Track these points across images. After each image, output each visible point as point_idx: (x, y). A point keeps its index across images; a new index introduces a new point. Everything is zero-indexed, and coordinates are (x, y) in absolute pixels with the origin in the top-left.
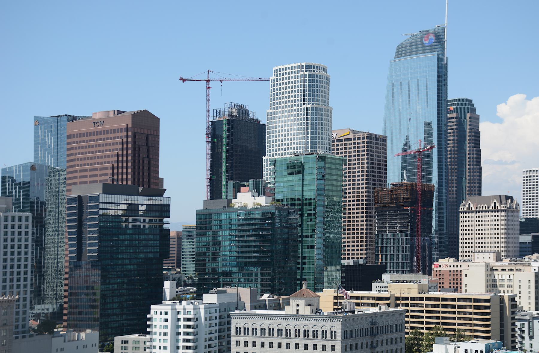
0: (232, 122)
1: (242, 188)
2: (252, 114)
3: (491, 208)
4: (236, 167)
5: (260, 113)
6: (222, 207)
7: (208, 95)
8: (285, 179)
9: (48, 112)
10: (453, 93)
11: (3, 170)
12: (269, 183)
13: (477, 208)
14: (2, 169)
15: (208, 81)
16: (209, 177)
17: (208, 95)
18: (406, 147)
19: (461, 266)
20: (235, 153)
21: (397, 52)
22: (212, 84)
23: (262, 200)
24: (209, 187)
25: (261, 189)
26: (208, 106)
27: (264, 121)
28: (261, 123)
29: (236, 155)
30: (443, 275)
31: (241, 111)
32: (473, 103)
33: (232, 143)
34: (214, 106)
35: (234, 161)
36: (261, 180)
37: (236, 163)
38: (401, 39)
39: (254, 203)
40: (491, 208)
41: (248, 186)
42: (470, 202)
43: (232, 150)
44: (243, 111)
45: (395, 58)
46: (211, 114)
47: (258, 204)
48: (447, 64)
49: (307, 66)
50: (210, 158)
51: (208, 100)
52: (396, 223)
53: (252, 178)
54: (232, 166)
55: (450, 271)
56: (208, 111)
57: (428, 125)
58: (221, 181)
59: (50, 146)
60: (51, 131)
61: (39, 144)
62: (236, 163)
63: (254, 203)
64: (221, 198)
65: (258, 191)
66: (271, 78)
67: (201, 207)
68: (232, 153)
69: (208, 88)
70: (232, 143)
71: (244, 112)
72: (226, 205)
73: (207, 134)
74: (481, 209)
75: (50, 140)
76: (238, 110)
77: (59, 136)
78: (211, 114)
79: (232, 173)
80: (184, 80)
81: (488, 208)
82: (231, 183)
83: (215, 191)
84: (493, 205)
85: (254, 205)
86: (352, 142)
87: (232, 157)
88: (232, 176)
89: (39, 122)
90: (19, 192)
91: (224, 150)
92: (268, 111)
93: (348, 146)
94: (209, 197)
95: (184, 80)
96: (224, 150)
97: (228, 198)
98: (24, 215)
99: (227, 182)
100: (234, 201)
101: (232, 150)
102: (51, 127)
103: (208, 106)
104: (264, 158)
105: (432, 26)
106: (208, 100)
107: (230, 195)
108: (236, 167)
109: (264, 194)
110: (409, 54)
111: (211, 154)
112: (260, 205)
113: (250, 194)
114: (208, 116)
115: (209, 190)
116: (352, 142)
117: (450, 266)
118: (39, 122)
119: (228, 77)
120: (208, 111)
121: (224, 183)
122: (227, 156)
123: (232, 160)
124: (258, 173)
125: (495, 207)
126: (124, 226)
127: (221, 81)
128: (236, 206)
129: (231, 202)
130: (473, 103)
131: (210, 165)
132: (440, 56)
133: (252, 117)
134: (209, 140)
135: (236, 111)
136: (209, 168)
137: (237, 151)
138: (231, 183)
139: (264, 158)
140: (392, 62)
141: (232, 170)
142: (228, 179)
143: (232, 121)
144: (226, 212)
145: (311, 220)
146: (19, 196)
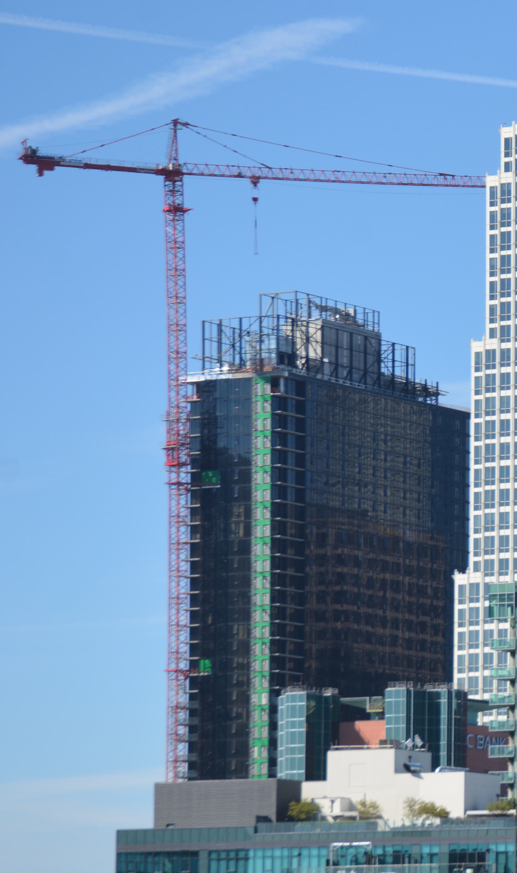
0: (301, 396)
2: (399, 355)
4: (320, 616)
6: (252, 822)
7: (176, 246)
12: (484, 706)
15: (172, 175)
16: (184, 665)
17: (176, 246)
20: (313, 550)
21: (168, 442)
22: (191, 189)
23: (447, 789)
24: (183, 715)
25: (443, 734)
26: (178, 300)
27: (455, 396)
28: (444, 401)
29: (322, 560)
31: (345, 339)
33: (300, 495)
35: (312, 588)
36: (442, 689)
37: (321, 597)
39: (411, 804)
41: (381, 716)
43: (301, 531)
44: (355, 342)
46: (193, 347)
47: (429, 810)
50: (185, 567)
51: (177, 273)
53: (395, 679)
54: (298, 616)
56: (177, 328)
58: (245, 685)
62: (321, 597)
63: (411, 804)
64: (243, 771)
65: (432, 744)
66: (491, 181)
67: (144, 819)
68: (300, 548)
69: (177, 210)
70: (300, 495)
71: (359, 340)
72: (272, 813)
76: (331, 335)
78: (193, 347)
79: (299, 649)
80: (44, 163)
82: (294, 702)
83: (214, 738)
87: (300, 566)
88: (299, 666)
92: (477, 347)
94: (184, 768)
95: (44, 163)
97: (282, 774)
99: (274, 694)
100: (310, 791)
101: (301, 531)
104: (459, 579)
106: (177, 273)
107: (291, 761)
108: (320, 616)
109: (460, 760)
111: (194, 549)
112: (443, 815)
113: (389, 755)
115: (183, 730)
119: (278, 160)
120: (177, 328)
121: (260, 698)
122: (275, 563)
123: (300, 582)
124: (429, 652)
126: (289, 551)
127: (255, 181)
128: (330, 810)
129: (297, 797)
131: (186, 605)
133: (399, 372)
134: (185, 476)
135: (315, 332)
136: (185, 619)
137: (322, 540)
138: (294, 702)
139: (459, 579)
141: (299, 632)
142: (278, 683)
143: (299, 385)
144: (272, 846)
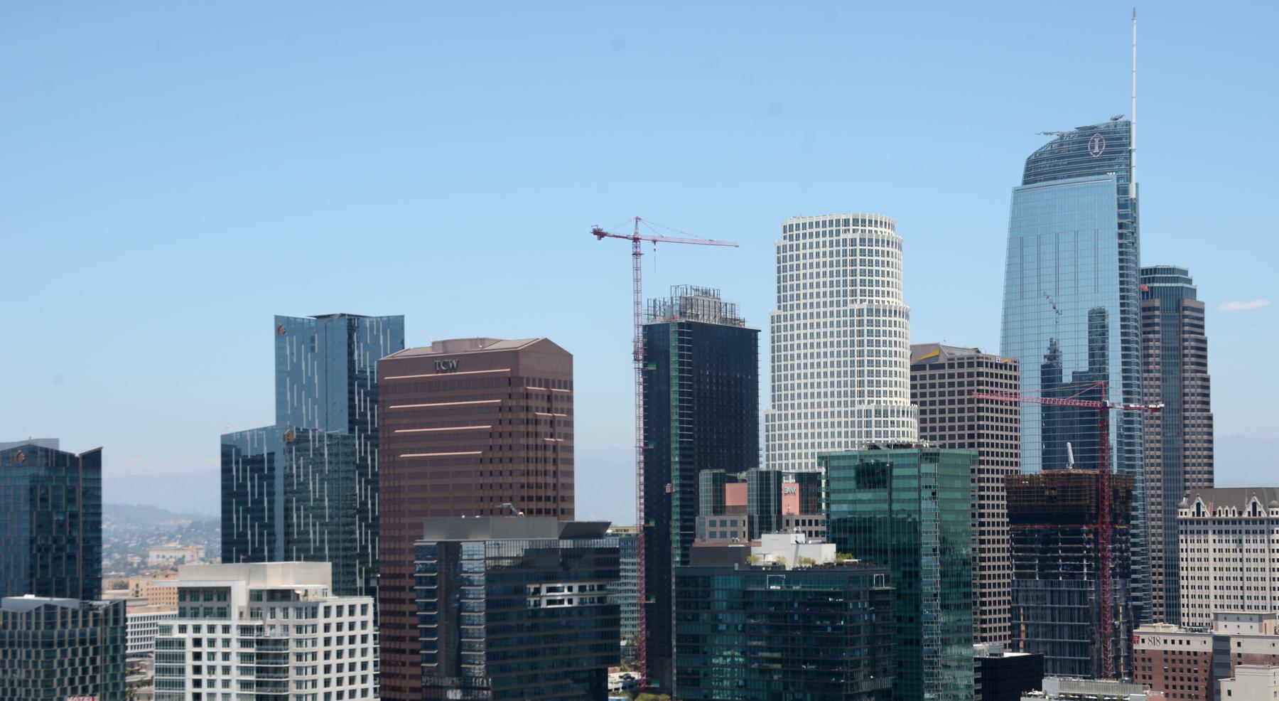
1: (727, 485)
3: (1245, 515)
5: (755, 311)
7: (637, 269)
8: (851, 497)
9: (305, 309)
10: (1148, 258)
11: (223, 437)
13: (1214, 513)
14: (223, 437)
15: (636, 240)
17: (637, 269)
18: (1050, 373)
19: (1188, 642)
22: (645, 246)
26: (637, 292)
30: (1150, 660)
32: (1190, 276)
34: (648, 295)
38: (1036, 143)
40: (1245, 515)
41: (744, 481)
42: (1199, 500)
45: (1025, 183)
48: (1137, 199)
49: (856, 221)
51: (637, 280)
52: (1056, 559)
55: (1166, 652)
56: (637, 303)
57: (1097, 320)
59: (311, 379)
60: (313, 349)
61: (286, 375)
73: (636, 353)
74: (1223, 516)
75: (309, 367)
77: (329, 360)
81: (1240, 513)
84: (1250, 509)
85: (801, 562)
86: (947, 371)
89: (284, 328)
90: (322, 533)
91: (675, 388)
93: (937, 381)
96: (675, 388)
98: (358, 601)
102: (313, 340)
103: (637, 292)
105: (1099, 117)
106: (637, 280)
110: (1052, 175)
114: (637, 315)
116: (947, 371)
117: (1165, 641)
118: (284, 328)
125: (1255, 514)
130: (1190, 276)
132: (1122, 182)
134: (641, 365)
140: (1017, 191)
145: (910, 585)
146: (322, 541)
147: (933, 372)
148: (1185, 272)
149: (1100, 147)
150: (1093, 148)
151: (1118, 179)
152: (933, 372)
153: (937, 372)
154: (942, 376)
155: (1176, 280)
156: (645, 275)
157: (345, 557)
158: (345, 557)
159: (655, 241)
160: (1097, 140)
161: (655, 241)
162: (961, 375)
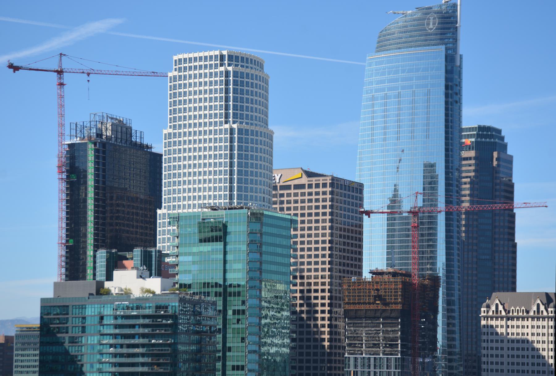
7: (61, 97)
15: (60, 72)
17: (61, 97)
26: (62, 115)
32: (503, 134)
40: (491, 313)
51: (61, 106)
56: (62, 125)
84: (535, 308)
106: (61, 106)
116: (307, 190)
125: (538, 312)
147: (282, 192)
148: (499, 131)
149: (434, 24)
150: (428, 24)
151: (447, 49)
152: (296, 191)
153: (285, 192)
154: (303, 194)
155: (491, 136)
156: (67, 101)
157: (419, 252)
158: (419, 252)
159: (88, 74)
160: (431, 18)
161: (88, 74)
162: (317, 193)
